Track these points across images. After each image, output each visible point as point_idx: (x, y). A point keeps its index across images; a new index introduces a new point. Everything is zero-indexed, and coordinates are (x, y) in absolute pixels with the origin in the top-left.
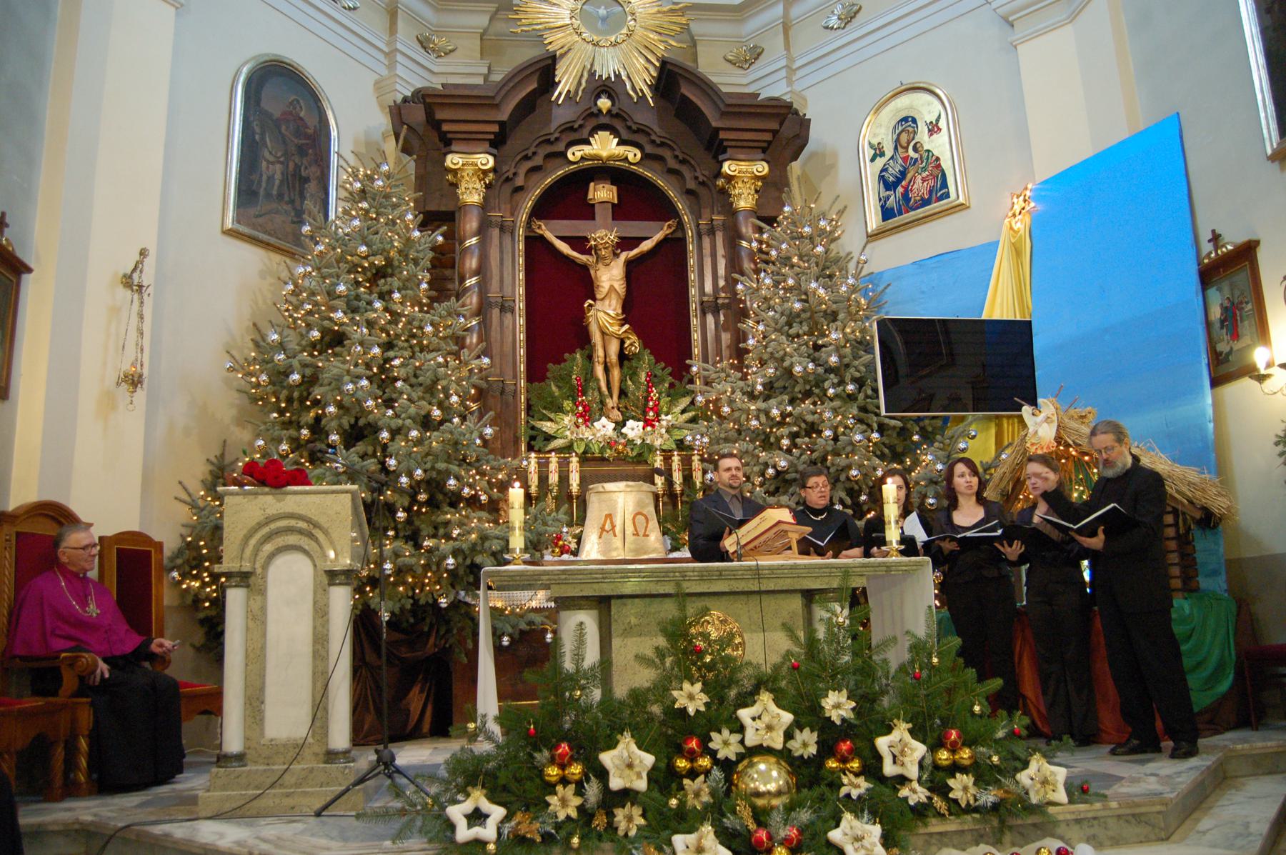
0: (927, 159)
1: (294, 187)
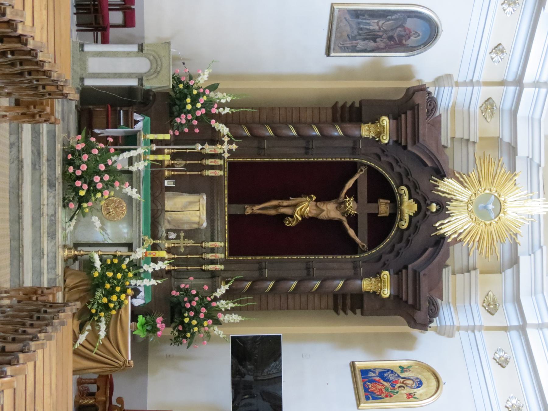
0: (393, 392)
1: (368, 35)
